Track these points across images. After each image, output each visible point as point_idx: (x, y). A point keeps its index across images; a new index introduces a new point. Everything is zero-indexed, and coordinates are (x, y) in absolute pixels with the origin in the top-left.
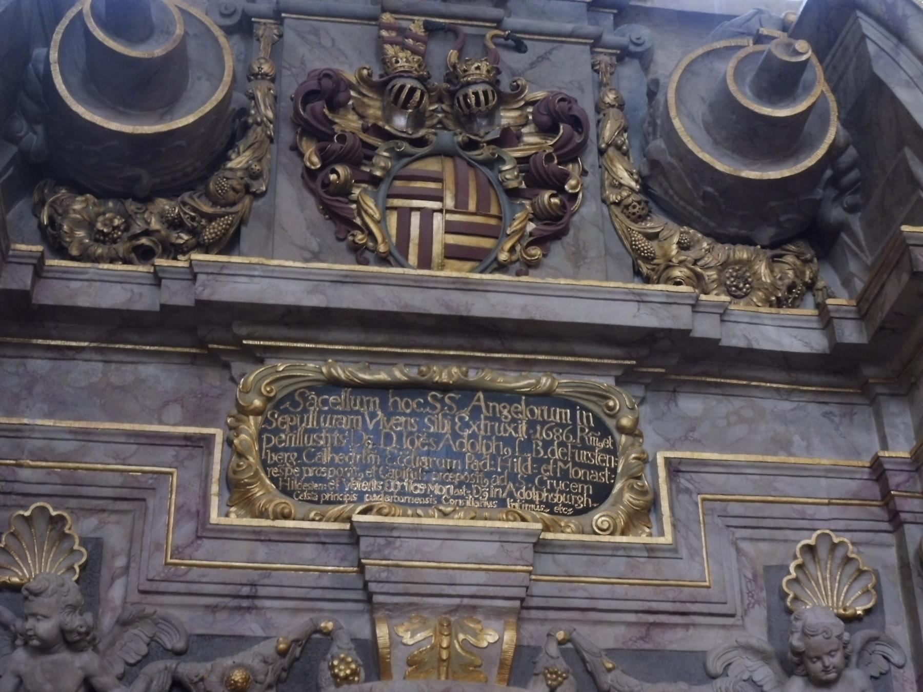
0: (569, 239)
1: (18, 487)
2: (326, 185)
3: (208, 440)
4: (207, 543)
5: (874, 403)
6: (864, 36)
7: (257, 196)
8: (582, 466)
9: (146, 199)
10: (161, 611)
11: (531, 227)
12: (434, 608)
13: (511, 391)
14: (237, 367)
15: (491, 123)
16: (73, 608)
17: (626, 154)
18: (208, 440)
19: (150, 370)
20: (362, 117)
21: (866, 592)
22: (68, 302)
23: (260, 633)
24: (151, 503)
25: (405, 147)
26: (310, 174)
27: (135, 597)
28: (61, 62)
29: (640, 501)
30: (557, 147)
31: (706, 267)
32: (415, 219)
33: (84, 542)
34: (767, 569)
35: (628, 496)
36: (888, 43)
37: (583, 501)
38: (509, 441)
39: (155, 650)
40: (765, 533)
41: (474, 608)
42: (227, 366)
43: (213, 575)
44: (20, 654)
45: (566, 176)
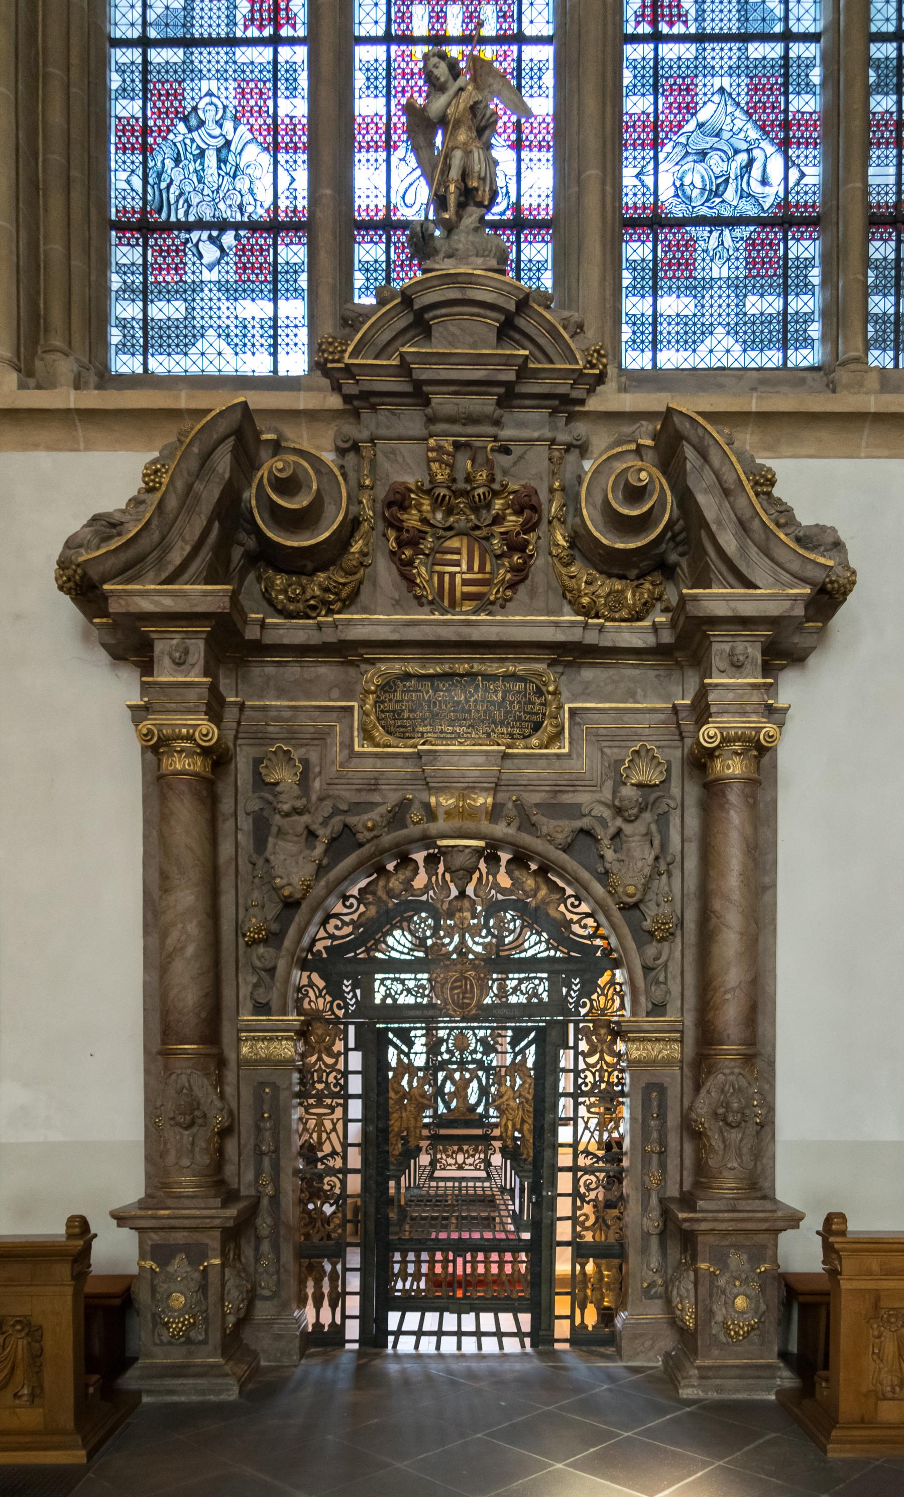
0: (528, 582)
1: (268, 735)
2: (401, 560)
3: (351, 708)
4: (355, 760)
5: (682, 668)
6: (686, 458)
7: (366, 566)
8: (528, 713)
9: (312, 573)
10: (336, 793)
11: (509, 576)
12: (456, 788)
13: (495, 675)
14: (363, 667)
15: (489, 511)
16: (298, 798)
17: (564, 523)
18: (351, 708)
19: (323, 670)
20: (420, 511)
21: (661, 772)
22: (278, 642)
23: (381, 801)
24: (329, 741)
25: (441, 532)
26: (393, 553)
27: (326, 787)
28: (258, 507)
29: (554, 730)
30: (523, 525)
31: (599, 597)
32: (447, 577)
33: (301, 760)
34: (616, 761)
35: (549, 728)
36: (699, 462)
37: (527, 732)
38: (492, 703)
39: (336, 811)
40: (616, 743)
41: (474, 788)
42: (358, 666)
43: (358, 775)
44: (277, 817)
45: (527, 542)
